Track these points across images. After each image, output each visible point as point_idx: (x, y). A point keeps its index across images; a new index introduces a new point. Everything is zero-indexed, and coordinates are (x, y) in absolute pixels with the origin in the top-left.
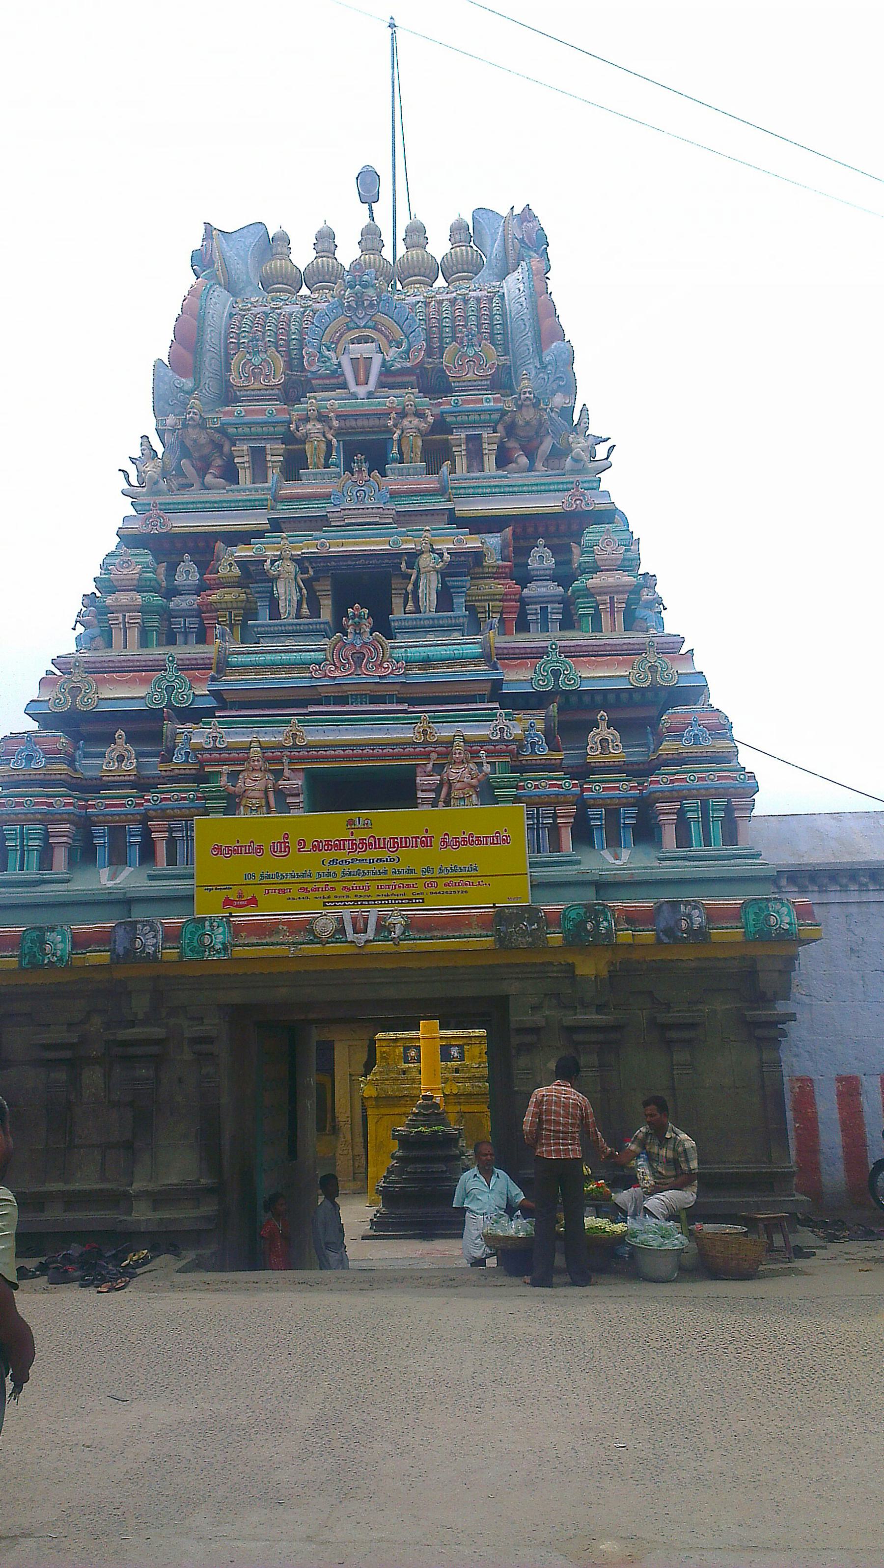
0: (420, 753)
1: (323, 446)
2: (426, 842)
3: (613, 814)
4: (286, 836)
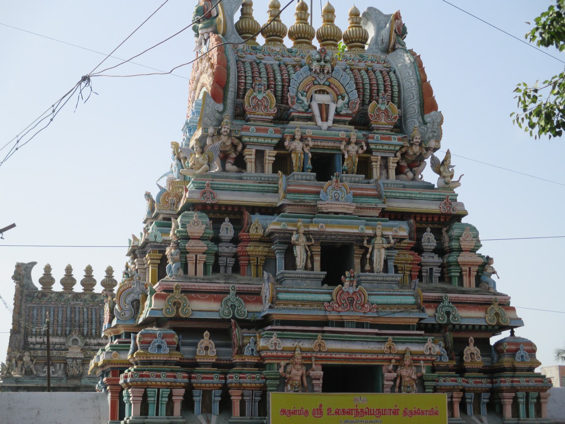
0: (386, 359)
1: (303, 156)
2: (396, 412)
3: (478, 396)
4: (321, 406)
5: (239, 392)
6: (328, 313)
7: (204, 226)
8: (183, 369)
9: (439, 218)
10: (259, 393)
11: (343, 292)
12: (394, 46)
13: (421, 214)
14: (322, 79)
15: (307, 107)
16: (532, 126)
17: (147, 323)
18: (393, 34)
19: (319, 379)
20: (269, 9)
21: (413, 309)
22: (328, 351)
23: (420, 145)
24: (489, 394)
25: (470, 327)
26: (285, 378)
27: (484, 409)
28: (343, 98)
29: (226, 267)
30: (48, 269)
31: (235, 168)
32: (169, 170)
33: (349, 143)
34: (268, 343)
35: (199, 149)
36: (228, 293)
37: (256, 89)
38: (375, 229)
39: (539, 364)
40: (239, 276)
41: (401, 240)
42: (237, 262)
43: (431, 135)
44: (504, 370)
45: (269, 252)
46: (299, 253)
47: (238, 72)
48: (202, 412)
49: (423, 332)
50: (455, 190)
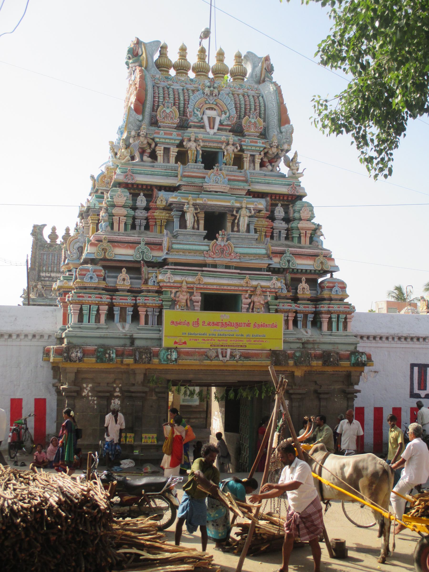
1: (196, 152)
2: (248, 325)
3: (306, 316)
4: (198, 319)
5: (145, 309)
6: (206, 259)
7: (125, 198)
8: (107, 293)
9: (288, 197)
10: (158, 310)
11: (217, 244)
12: (264, 79)
13: (276, 194)
14: (211, 100)
15: (200, 119)
16: (324, 126)
17: (86, 262)
18: (264, 71)
19: (198, 302)
20: (179, 51)
21: (264, 257)
22: (205, 284)
23: (277, 147)
24: (313, 315)
25: (304, 271)
26: (175, 301)
27: (309, 324)
28: (225, 113)
29: (140, 226)
30: (54, 229)
31: (149, 159)
32: (107, 160)
33: (228, 144)
34: (165, 277)
35: (124, 146)
36: (140, 243)
37: (165, 106)
38: (242, 203)
39: (347, 296)
40: (148, 232)
41: (260, 211)
42: (147, 223)
43: (285, 141)
44: (324, 299)
45: (169, 217)
46: (189, 218)
47: (154, 93)
48: (120, 321)
49: (270, 273)
50: (299, 179)
